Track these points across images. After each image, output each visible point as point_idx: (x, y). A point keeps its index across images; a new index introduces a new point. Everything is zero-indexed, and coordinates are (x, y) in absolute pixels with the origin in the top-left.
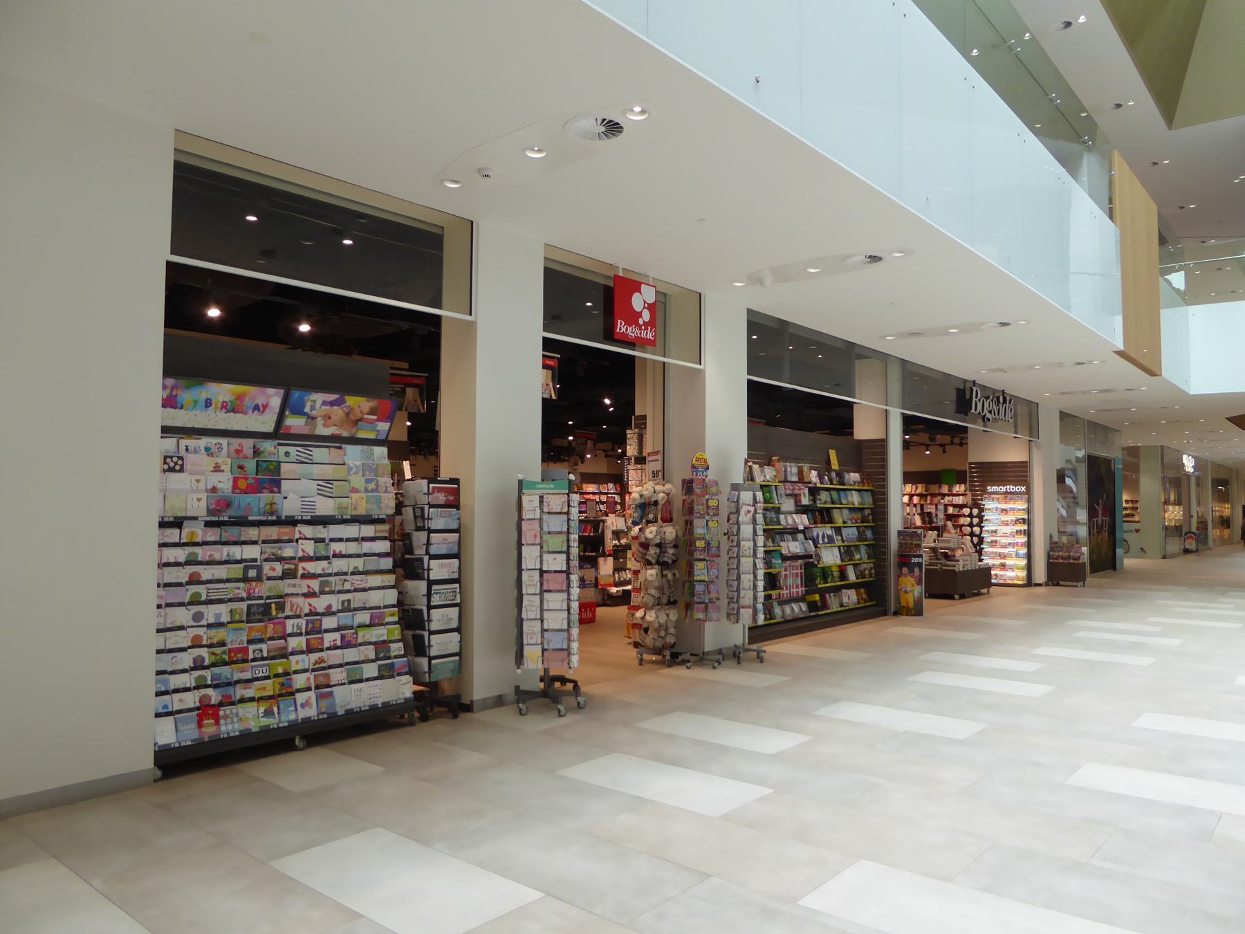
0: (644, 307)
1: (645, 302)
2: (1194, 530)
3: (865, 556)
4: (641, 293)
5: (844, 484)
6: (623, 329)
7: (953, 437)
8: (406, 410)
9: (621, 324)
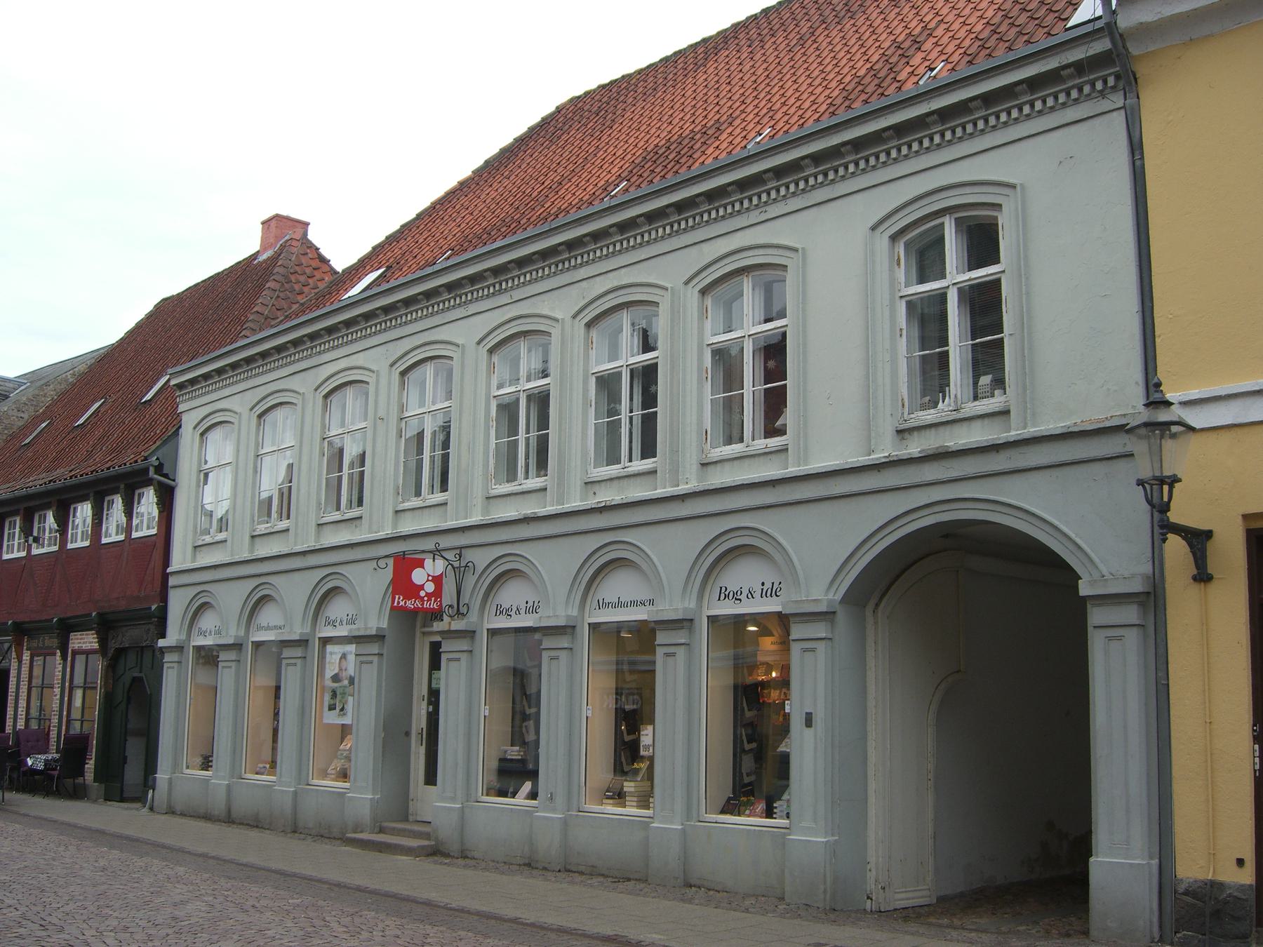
0: (428, 580)
1: (429, 575)
2: (406, 556)
3: (182, 869)
4: (424, 568)
5: (406, 819)
6: (402, 603)
7: (57, 531)
8: (1198, 540)
9: (399, 598)
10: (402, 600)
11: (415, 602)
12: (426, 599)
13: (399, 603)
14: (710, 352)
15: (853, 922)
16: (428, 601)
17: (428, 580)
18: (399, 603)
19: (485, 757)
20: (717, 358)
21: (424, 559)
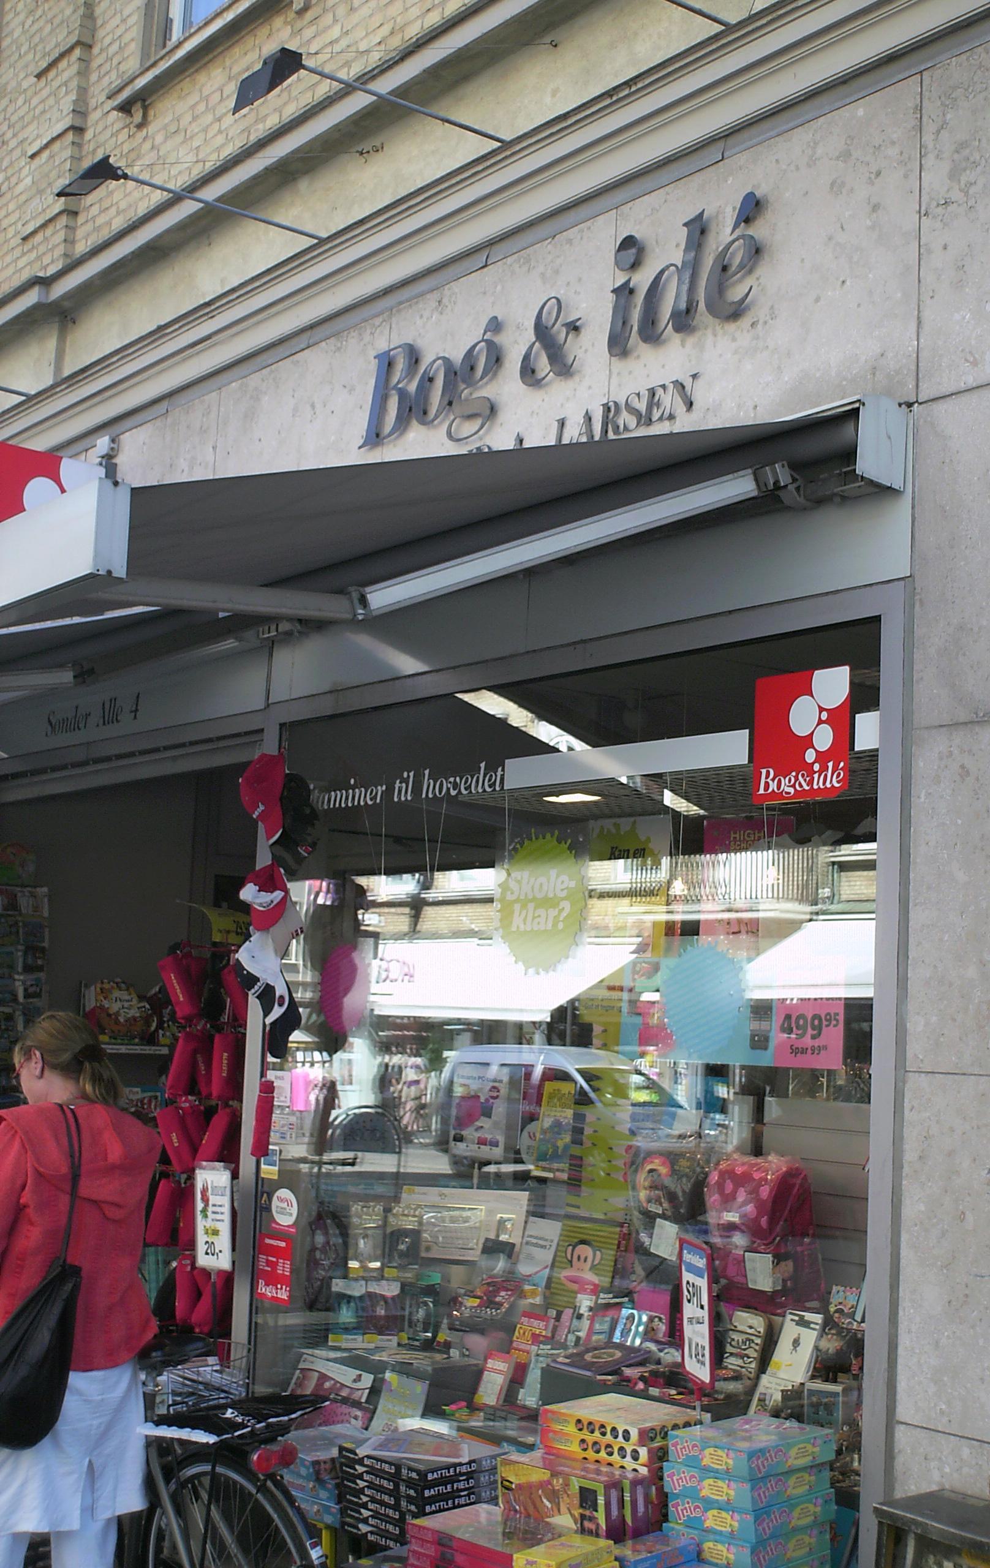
0: (820, 722)
1: (821, 709)
6: (773, 786)
9: (768, 773)
10: (773, 780)
11: (797, 778)
12: (816, 767)
13: (767, 785)
14: (240, 1176)
15: (416, 906)
16: (820, 772)
17: (820, 722)
18: (767, 785)
19: (288, 353)
20: (164, 1445)
21: (62, 458)
